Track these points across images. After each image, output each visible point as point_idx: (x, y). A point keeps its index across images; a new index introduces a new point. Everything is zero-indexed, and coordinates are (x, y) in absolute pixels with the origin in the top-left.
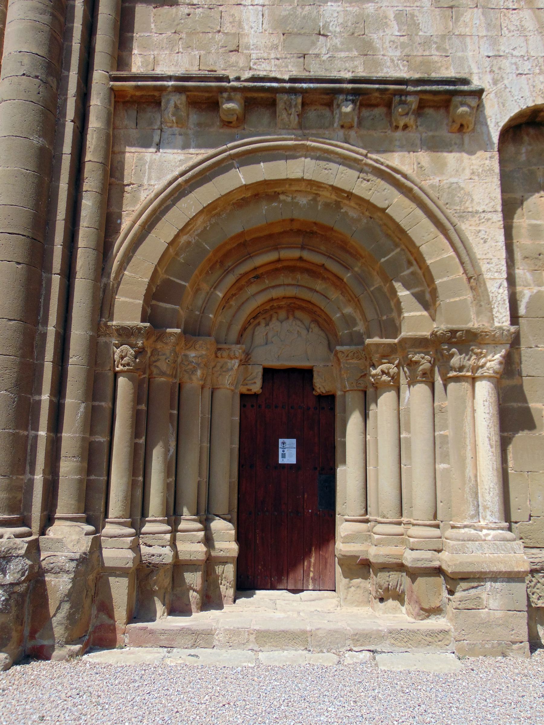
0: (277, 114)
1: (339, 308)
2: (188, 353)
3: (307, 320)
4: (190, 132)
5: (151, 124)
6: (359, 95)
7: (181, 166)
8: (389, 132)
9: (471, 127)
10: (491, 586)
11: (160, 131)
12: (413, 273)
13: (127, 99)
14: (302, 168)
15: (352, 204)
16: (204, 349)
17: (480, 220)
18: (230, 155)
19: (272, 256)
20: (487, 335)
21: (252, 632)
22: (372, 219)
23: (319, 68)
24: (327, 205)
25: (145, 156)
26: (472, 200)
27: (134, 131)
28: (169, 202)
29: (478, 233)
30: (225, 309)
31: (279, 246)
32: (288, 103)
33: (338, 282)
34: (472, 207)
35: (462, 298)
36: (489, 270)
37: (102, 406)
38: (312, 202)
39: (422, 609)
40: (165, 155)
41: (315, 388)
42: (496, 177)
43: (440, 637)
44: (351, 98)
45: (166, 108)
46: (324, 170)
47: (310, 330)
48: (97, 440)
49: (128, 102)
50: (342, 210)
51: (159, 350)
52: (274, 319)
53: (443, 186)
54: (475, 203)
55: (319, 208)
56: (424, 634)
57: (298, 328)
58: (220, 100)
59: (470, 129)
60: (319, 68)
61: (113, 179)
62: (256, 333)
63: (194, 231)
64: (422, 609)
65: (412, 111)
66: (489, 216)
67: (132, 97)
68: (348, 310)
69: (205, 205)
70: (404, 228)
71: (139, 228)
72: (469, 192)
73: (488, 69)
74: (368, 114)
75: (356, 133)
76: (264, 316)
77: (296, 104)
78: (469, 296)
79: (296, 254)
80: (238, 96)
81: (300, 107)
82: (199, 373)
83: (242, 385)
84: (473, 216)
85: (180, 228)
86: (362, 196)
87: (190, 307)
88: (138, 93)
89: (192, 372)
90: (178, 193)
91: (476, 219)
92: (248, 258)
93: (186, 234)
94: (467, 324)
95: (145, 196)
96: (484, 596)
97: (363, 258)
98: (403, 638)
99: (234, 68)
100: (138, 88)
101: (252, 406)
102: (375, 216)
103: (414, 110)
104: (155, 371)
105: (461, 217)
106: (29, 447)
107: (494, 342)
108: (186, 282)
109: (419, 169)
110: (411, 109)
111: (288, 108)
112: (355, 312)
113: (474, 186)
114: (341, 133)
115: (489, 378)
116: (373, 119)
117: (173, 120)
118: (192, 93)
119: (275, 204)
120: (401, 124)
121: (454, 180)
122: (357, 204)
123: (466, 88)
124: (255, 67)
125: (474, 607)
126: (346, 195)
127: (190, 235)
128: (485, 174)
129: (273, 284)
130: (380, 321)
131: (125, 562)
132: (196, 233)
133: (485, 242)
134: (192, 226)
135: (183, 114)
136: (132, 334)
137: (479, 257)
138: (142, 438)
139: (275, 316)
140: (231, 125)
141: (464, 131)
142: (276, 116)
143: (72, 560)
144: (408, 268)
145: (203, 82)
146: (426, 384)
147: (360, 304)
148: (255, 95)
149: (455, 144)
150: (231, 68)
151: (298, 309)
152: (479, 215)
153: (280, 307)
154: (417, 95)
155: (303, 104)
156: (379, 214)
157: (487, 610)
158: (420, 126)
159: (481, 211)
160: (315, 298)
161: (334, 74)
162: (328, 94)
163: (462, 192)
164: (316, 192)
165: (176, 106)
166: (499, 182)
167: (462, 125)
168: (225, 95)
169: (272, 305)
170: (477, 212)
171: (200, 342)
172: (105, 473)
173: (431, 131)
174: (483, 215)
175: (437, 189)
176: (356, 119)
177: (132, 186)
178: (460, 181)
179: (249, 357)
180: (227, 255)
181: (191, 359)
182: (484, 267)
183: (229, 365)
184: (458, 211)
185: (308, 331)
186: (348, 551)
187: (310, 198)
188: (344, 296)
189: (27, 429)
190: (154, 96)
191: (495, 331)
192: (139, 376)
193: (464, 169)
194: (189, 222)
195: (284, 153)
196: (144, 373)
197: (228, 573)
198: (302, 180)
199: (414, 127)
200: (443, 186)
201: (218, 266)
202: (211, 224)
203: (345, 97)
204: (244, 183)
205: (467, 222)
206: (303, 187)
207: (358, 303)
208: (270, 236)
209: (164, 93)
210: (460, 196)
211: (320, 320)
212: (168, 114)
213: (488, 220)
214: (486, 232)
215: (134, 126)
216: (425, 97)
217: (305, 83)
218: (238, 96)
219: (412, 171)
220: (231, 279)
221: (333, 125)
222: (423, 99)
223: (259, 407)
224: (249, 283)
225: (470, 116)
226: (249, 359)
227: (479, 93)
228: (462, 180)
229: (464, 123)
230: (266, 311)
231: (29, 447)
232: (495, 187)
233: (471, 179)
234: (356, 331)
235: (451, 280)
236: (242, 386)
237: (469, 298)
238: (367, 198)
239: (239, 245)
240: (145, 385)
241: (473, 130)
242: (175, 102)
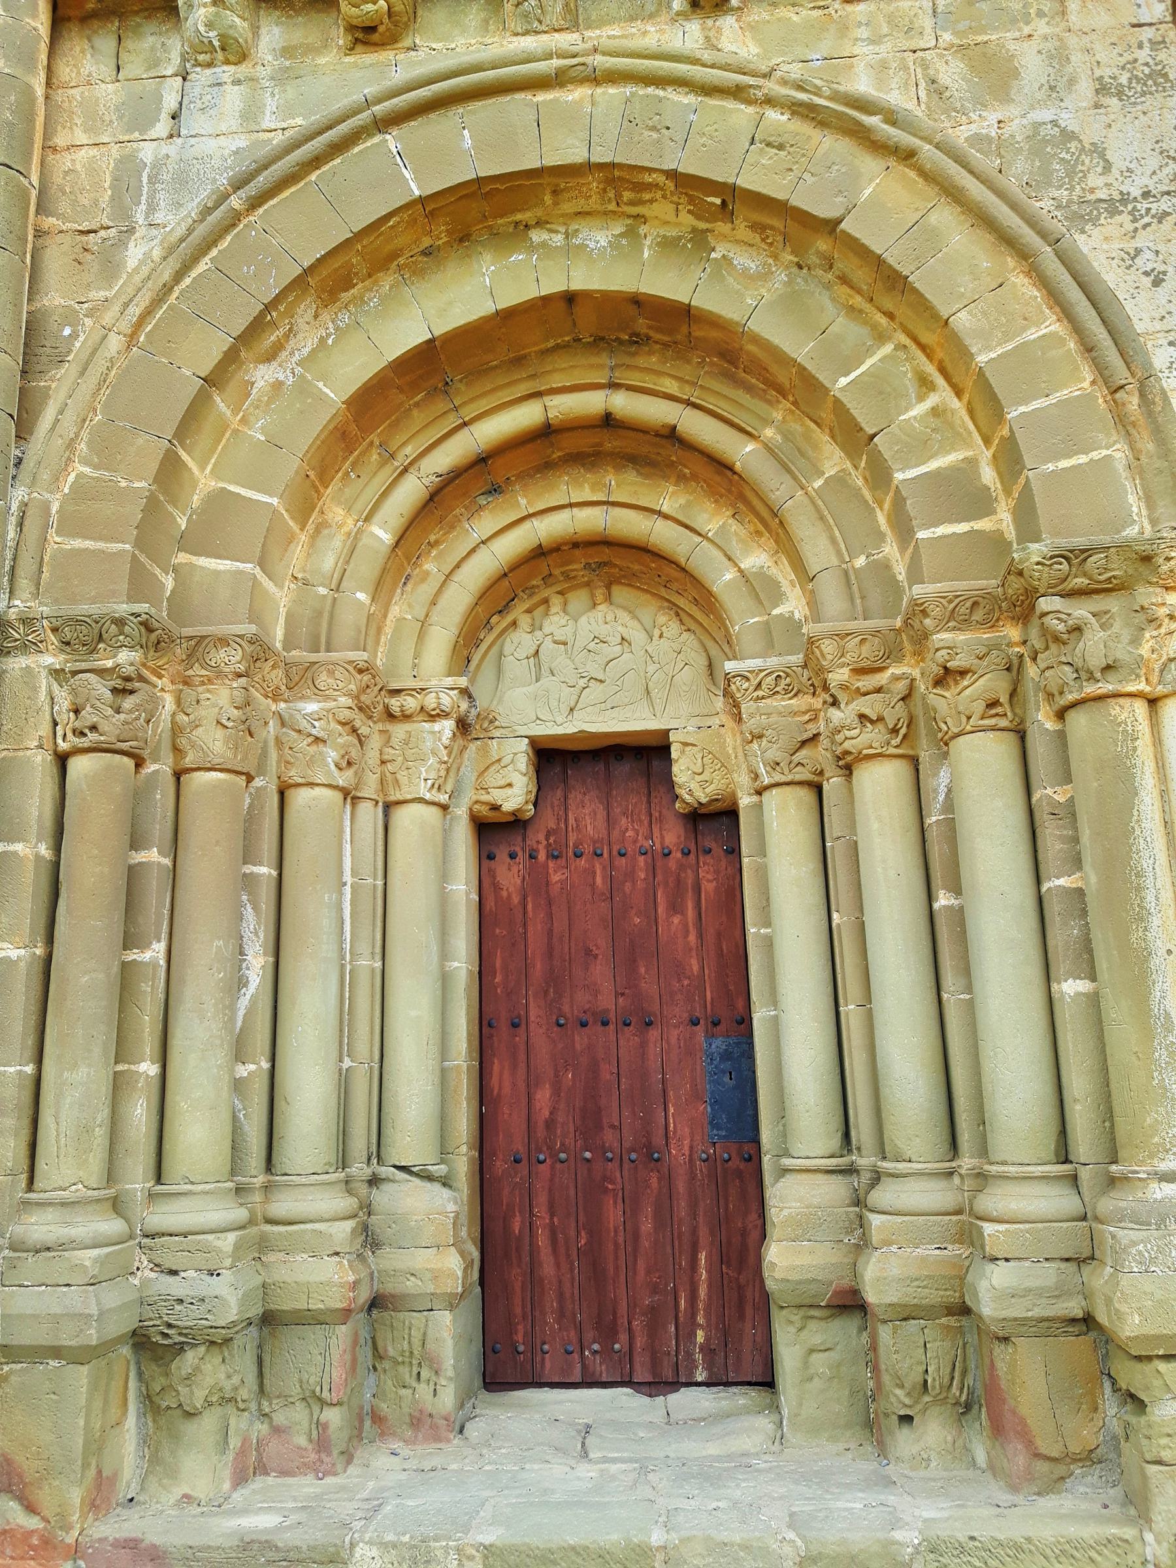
4: (261, 72)
12: (935, 411)
17: (1135, 220)
25: (138, 150)
26: (1108, 167)
35: (1095, 455)
37: (15, 853)
40: (193, 141)
50: (713, 255)
54: (1115, 171)
63: (292, 354)
68: (756, 559)
69: (306, 265)
78: (1118, 446)
84: (1113, 212)
101: (512, 856)
109: (935, 97)
121: (1045, 115)
130: (846, 573)
133: (1157, 283)
134: (279, 333)
136: (101, 638)
137: (1139, 327)
140: (375, 37)
144: (921, 399)
149: (1040, 14)
159: (1136, 192)
160: (662, 534)
170: (1125, 199)
174: (1142, 206)
177: (102, 233)
193: (1072, 81)
197: (448, 1335)
202: (337, 329)
204: (417, 193)
205: (1095, 232)
210: (1068, 157)
215: (107, 70)
220: (410, 492)
223: (531, 857)
237: (1118, 455)
238: (781, 196)
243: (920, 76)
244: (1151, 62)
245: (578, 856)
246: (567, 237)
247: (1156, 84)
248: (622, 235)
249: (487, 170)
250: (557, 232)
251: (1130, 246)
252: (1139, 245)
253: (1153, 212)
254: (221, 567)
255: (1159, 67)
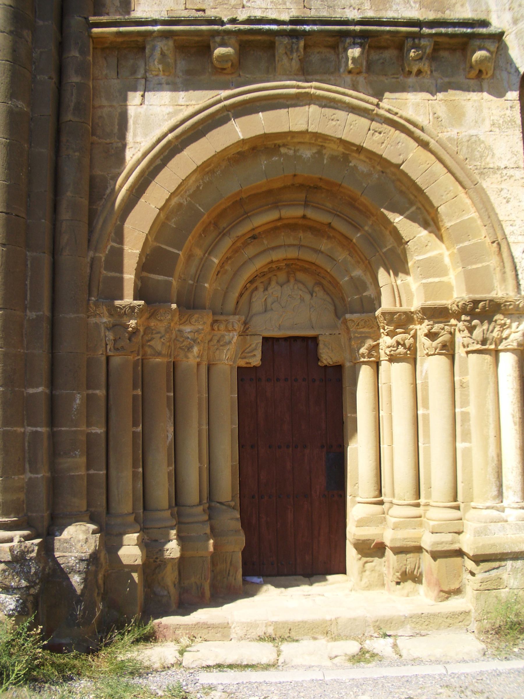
0: (277, 59)
1: (346, 271)
2: (182, 327)
3: (309, 281)
5: (134, 72)
6: (368, 37)
7: (170, 119)
8: (401, 78)
9: (490, 73)
10: (512, 566)
11: (144, 80)
13: (106, 45)
14: (306, 119)
15: (362, 157)
16: (201, 323)
17: (502, 177)
18: (225, 106)
19: (273, 216)
20: (510, 305)
21: (271, 624)
22: (384, 174)
23: (321, 5)
24: (333, 158)
26: (493, 155)
27: (116, 81)
28: (158, 162)
29: (500, 192)
30: (219, 275)
31: (279, 204)
32: (289, 47)
33: (346, 242)
34: (493, 163)
35: (484, 264)
36: (513, 233)
37: (96, 394)
38: (317, 156)
39: (442, 591)
40: (151, 107)
41: (321, 359)
42: (517, 129)
43: (460, 618)
44: (359, 41)
45: (151, 55)
46: (331, 122)
47: (314, 295)
48: (94, 431)
49: (107, 48)
50: (350, 164)
51: (153, 328)
52: (273, 283)
53: (462, 139)
55: (325, 162)
56: (444, 616)
57: (300, 293)
58: (212, 45)
59: (489, 75)
60: (321, 5)
61: (95, 138)
62: (254, 300)
64: (442, 591)
65: (426, 55)
66: (511, 172)
67: (111, 43)
70: (421, 186)
71: (126, 193)
72: (489, 146)
73: (507, 7)
74: (377, 57)
75: (365, 78)
76: (263, 280)
77: (298, 48)
79: (299, 212)
80: (233, 40)
81: (302, 50)
82: (196, 350)
83: (240, 358)
84: (495, 173)
85: (172, 191)
86: (374, 150)
87: (182, 276)
88: (120, 40)
89: (188, 349)
90: (167, 151)
91: (498, 176)
92: (246, 218)
93: (177, 196)
94: (490, 293)
95: (131, 156)
96: (505, 576)
97: (373, 215)
98: (423, 624)
99: (225, 6)
100: (119, 34)
102: (388, 171)
103: (428, 54)
104: (149, 351)
105: (481, 174)
106: (26, 444)
107: (518, 312)
108: (179, 250)
109: (436, 120)
110: (425, 53)
111: (289, 53)
112: (365, 274)
113: (495, 140)
114: (348, 78)
115: (513, 351)
116: (383, 63)
117: (159, 69)
118: (181, 37)
119: (275, 158)
120: (415, 69)
121: (473, 132)
122: (367, 157)
123: (484, 30)
124: (249, 4)
125: (495, 587)
126: (355, 149)
127: (181, 196)
128: (506, 126)
129: (273, 245)
131: (133, 559)
132: (188, 193)
133: (508, 202)
135: (171, 60)
138: (139, 426)
139: (274, 278)
140: (225, 72)
141: (483, 77)
142: (275, 61)
143: (82, 560)
145: (193, 25)
146: (447, 357)
147: (371, 266)
148: (251, 38)
150: (222, 6)
151: (299, 270)
152: (500, 172)
153: (279, 269)
154: (431, 38)
155: (305, 47)
156: (393, 169)
157: (507, 589)
158: (435, 71)
159: (503, 167)
161: (338, 14)
162: (334, 36)
163: (482, 145)
164: (321, 144)
165: (163, 54)
166: (522, 135)
167: (480, 71)
168: (218, 39)
169: (270, 267)
171: (196, 316)
172: (104, 467)
173: (447, 77)
174: (505, 172)
175: (456, 143)
176: (364, 63)
178: (479, 133)
179: (247, 326)
180: (222, 215)
181: (186, 335)
182: (508, 230)
183: (227, 338)
184: (479, 167)
185: (312, 295)
186: (362, 536)
187: (314, 150)
188: (352, 257)
189: (23, 426)
190: (137, 41)
191: (519, 300)
192: (133, 358)
193: (483, 120)
194: (181, 183)
195: (285, 101)
196: (138, 355)
198: (306, 132)
199: (429, 72)
200: (462, 139)
201: (212, 228)
202: (204, 182)
203: (352, 40)
204: (242, 137)
206: (307, 139)
207: (369, 266)
208: (270, 192)
209: (149, 39)
210: (480, 150)
211: (325, 282)
212: (154, 61)
213: (511, 177)
214: (508, 191)
215: (115, 76)
216: (440, 40)
217: (308, 25)
218: (233, 40)
219: (428, 121)
221: (339, 70)
222: (438, 42)
224: (245, 244)
225: (489, 62)
226: (247, 329)
227: (499, 37)
228: (481, 131)
229: (483, 69)
230: (264, 274)
231: (26, 444)
232: (518, 140)
233: (491, 131)
234: (366, 295)
235: (472, 244)
236: (240, 360)
238: (380, 153)
239: (235, 203)
240: (140, 368)
241: (493, 76)
242: (161, 49)
243: (430, 110)
244: (511, 116)
245: (278, 380)
246: (295, 152)
247: (512, 125)
248: (316, 153)
249: (267, 131)
250: (290, 149)
251: (500, 187)
252: (503, 187)
253: (508, 175)
254: (160, 279)
255: (513, 118)
